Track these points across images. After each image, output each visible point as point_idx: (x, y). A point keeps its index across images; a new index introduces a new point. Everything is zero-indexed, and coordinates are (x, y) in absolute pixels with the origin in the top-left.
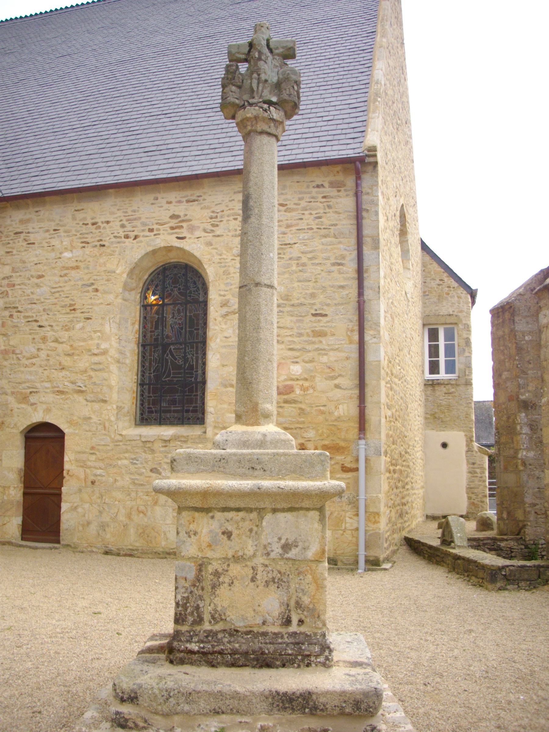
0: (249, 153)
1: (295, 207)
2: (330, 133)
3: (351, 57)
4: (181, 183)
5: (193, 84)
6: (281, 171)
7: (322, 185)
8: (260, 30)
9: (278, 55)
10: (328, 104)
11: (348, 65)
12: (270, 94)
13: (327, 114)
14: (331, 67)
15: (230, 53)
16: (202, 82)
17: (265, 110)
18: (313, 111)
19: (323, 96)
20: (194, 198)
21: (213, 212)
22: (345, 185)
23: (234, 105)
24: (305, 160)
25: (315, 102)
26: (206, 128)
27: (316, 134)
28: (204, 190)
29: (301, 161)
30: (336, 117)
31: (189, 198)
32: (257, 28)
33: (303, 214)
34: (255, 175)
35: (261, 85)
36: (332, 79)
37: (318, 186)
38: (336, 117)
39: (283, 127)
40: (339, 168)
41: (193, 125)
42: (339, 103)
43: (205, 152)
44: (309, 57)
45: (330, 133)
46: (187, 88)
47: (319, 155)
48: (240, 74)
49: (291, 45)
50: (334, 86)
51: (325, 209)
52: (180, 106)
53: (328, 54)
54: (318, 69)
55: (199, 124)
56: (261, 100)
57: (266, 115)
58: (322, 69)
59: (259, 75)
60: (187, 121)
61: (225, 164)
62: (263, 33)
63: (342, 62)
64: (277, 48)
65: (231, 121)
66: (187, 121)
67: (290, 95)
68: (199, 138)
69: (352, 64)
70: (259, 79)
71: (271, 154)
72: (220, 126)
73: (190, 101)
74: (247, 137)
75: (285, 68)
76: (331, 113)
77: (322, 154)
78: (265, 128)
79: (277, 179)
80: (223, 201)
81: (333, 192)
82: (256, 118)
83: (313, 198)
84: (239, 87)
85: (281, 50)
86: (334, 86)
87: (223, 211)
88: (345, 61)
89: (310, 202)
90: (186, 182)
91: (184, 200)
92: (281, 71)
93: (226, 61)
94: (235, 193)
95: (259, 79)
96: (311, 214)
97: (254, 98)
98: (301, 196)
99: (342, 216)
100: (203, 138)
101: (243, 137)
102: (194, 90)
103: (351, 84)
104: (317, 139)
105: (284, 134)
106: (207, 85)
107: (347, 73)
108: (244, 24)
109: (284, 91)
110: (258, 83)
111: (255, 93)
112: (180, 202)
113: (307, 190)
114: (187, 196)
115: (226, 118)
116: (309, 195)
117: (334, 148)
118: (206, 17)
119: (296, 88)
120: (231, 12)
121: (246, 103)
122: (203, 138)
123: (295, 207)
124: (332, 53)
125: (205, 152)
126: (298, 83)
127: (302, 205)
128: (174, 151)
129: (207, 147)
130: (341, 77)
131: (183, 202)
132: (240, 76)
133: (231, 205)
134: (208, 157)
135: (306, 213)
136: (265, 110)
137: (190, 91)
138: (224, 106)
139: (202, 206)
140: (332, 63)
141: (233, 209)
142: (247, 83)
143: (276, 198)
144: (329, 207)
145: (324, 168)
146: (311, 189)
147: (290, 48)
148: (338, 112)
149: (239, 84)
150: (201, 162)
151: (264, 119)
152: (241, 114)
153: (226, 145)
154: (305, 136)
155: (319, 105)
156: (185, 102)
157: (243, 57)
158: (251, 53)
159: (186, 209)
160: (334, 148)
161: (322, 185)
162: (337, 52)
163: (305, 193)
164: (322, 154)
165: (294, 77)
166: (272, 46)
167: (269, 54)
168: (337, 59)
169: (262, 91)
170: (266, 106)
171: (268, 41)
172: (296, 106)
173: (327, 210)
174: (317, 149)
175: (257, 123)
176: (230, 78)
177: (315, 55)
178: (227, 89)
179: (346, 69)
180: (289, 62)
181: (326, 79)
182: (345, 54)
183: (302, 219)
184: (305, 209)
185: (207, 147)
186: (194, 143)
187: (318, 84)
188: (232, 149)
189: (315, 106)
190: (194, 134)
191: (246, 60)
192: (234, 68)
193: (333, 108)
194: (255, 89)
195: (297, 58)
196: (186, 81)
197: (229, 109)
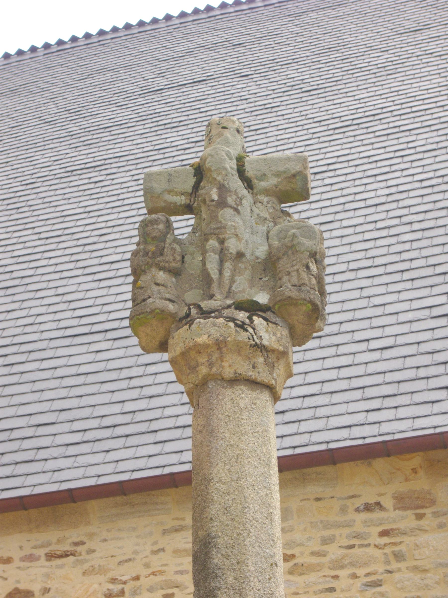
0: (204, 434)
1: (314, 560)
2: (389, 377)
3: (426, 199)
4: (33, 512)
5: (57, 276)
6: (288, 475)
7: (378, 504)
8: (220, 135)
9: (266, 192)
10: (379, 311)
11: (421, 217)
12: (252, 286)
13: (378, 333)
14: (380, 225)
15: (149, 194)
16: (79, 272)
17: (242, 326)
18: (345, 327)
19: (366, 293)
20: (67, 547)
21: (113, 581)
22: (433, 502)
23: (163, 315)
24: (333, 446)
25: (347, 306)
26: (91, 379)
27: (356, 383)
28: (90, 529)
29: (323, 447)
30: (401, 340)
31: (53, 547)
32: (214, 131)
33: (336, 577)
34: (223, 487)
35: (227, 265)
36: (384, 251)
37: (368, 508)
38: (401, 340)
39: (288, 366)
40: (416, 460)
41: (59, 372)
42: (405, 306)
43: (90, 436)
44: (327, 203)
45: (389, 377)
46: (44, 285)
47: (367, 431)
48: (176, 241)
49: (298, 168)
50: (390, 269)
51: (388, 562)
52: (29, 329)
53: (372, 194)
54: (351, 231)
55: (73, 370)
56: (229, 302)
57: (243, 336)
58: (359, 229)
59: (222, 242)
60: (46, 364)
61: (141, 463)
62: (227, 142)
63: (406, 211)
64: (263, 177)
65: (157, 357)
66: (46, 364)
67: (300, 286)
68: (75, 403)
69: (429, 215)
70: (222, 253)
71: (262, 432)
72: (125, 373)
73: (51, 317)
74: (198, 392)
75: (284, 223)
76: (389, 331)
77: (374, 429)
78: (243, 368)
79: (277, 496)
80: (136, 552)
81: (407, 520)
82: (220, 345)
83: (357, 536)
84: (176, 273)
85: (273, 181)
86: (390, 269)
87: (137, 578)
88: (413, 210)
89: (351, 547)
90: (45, 510)
91: (42, 552)
92: (275, 230)
93: (140, 213)
94: (165, 532)
95: (222, 253)
96: (354, 576)
97: (211, 297)
98: (327, 533)
99: (431, 578)
100: (84, 401)
101: (190, 393)
102: (60, 291)
103: (432, 261)
104: (357, 394)
105: (289, 382)
106: (90, 278)
107: (419, 235)
108: (172, 137)
109: (285, 278)
110: (222, 262)
111: (215, 285)
112: (31, 558)
113: (341, 519)
114: (49, 544)
115: (147, 350)
116: (346, 531)
117: (402, 413)
118: (85, 124)
119: (314, 268)
120: (143, 111)
121: (194, 311)
122: (84, 401)
123: (314, 560)
124: (379, 192)
125: (90, 436)
126: (316, 257)
127: (331, 556)
128: (16, 434)
129: (95, 423)
130: (407, 246)
131: (38, 559)
132: (175, 246)
133: (156, 562)
134: (98, 446)
135: (342, 573)
136: (242, 326)
137: (52, 292)
138: (141, 317)
139: (86, 566)
140: (383, 216)
141: (161, 572)
142: (194, 262)
143: (279, 544)
144: (399, 557)
145: (380, 463)
146: (352, 515)
147: (294, 176)
148: (405, 328)
149: (173, 264)
150: (81, 460)
151: (239, 348)
152: (181, 338)
153: (140, 417)
154: (328, 387)
155: (359, 314)
156: (40, 319)
157: (182, 200)
158: (201, 192)
159: (47, 576)
160: (402, 413)
161: (378, 504)
162: (393, 190)
163: (338, 525)
164: (374, 429)
165: (307, 243)
166: (250, 172)
167: (244, 192)
168: (394, 205)
169: (232, 281)
170: (242, 316)
171: (240, 160)
172: (316, 313)
173: (394, 565)
174: (360, 418)
175: (221, 358)
176: (152, 252)
177: (342, 200)
178: (144, 279)
179: (416, 226)
180: (297, 210)
181: (370, 253)
182: (412, 194)
183: (332, 590)
184: (338, 564)
185: (95, 423)
186: (64, 416)
187: (353, 266)
188: (155, 426)
189: (349, 315)
190: (63, 393)
191: (188, 209)
192: (161, 226)
193: (392, 319)
194: (214, 275)
195: (312, 199)
196: (40, 271)
197: (153, 326)
